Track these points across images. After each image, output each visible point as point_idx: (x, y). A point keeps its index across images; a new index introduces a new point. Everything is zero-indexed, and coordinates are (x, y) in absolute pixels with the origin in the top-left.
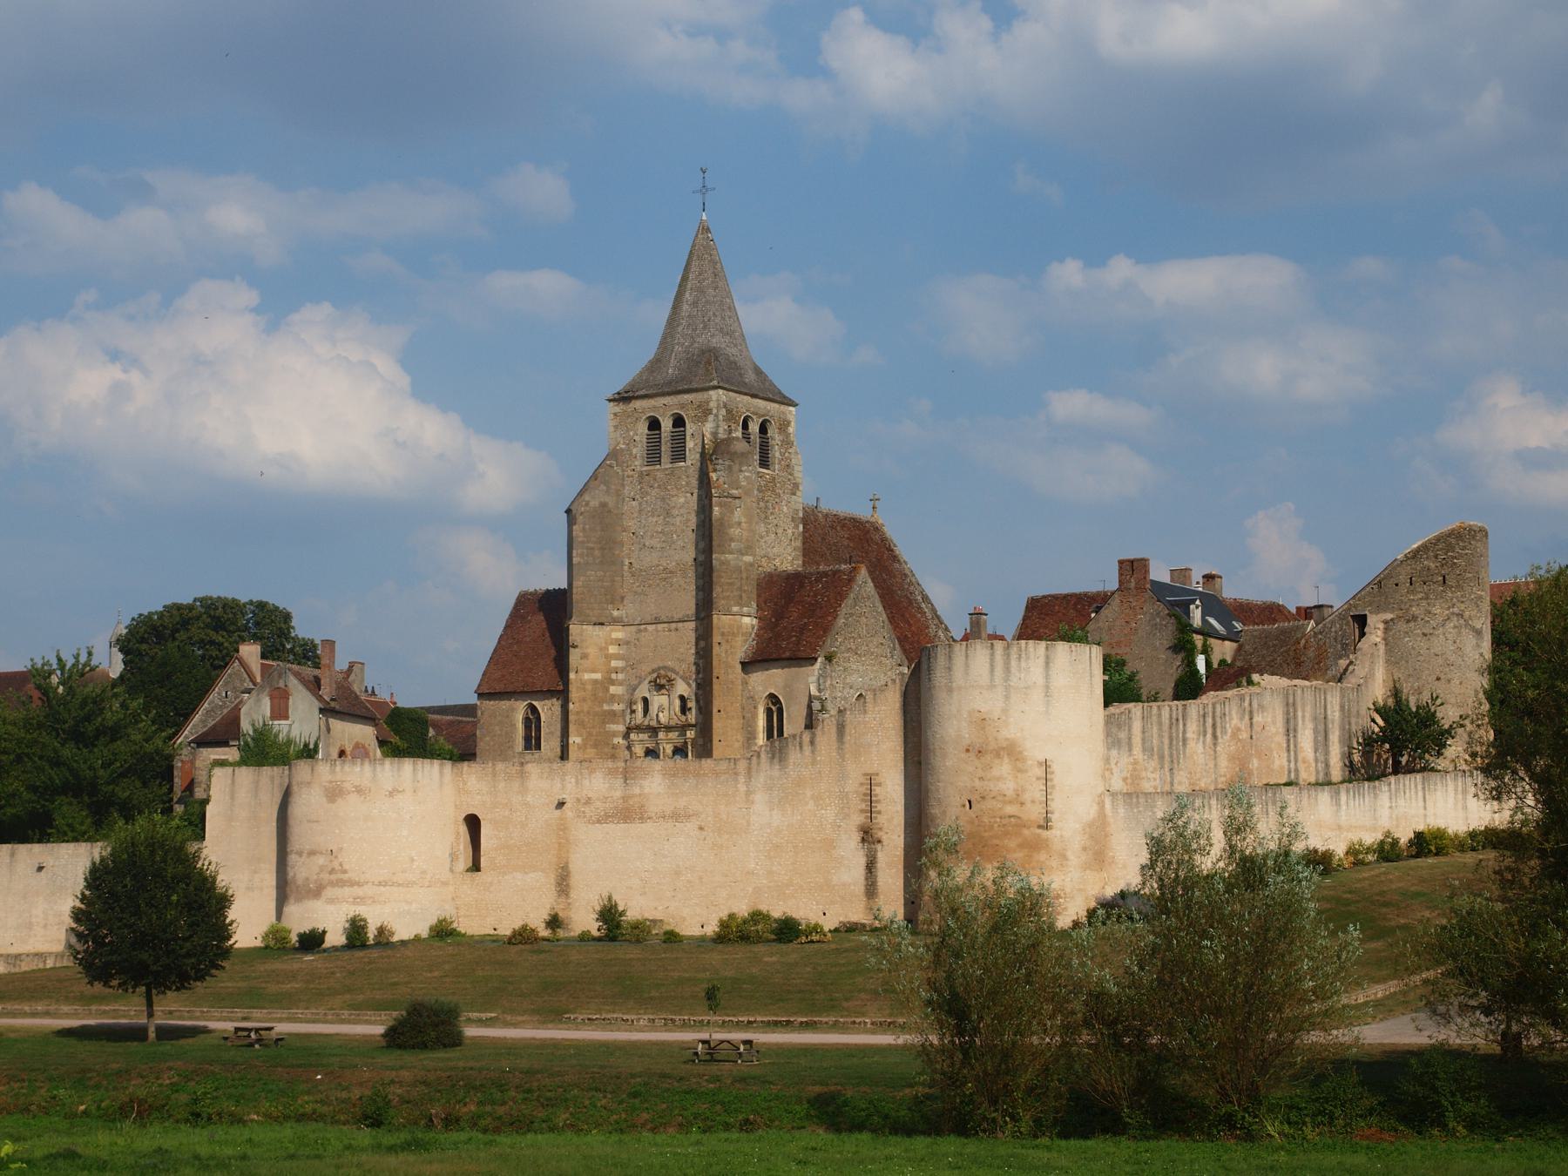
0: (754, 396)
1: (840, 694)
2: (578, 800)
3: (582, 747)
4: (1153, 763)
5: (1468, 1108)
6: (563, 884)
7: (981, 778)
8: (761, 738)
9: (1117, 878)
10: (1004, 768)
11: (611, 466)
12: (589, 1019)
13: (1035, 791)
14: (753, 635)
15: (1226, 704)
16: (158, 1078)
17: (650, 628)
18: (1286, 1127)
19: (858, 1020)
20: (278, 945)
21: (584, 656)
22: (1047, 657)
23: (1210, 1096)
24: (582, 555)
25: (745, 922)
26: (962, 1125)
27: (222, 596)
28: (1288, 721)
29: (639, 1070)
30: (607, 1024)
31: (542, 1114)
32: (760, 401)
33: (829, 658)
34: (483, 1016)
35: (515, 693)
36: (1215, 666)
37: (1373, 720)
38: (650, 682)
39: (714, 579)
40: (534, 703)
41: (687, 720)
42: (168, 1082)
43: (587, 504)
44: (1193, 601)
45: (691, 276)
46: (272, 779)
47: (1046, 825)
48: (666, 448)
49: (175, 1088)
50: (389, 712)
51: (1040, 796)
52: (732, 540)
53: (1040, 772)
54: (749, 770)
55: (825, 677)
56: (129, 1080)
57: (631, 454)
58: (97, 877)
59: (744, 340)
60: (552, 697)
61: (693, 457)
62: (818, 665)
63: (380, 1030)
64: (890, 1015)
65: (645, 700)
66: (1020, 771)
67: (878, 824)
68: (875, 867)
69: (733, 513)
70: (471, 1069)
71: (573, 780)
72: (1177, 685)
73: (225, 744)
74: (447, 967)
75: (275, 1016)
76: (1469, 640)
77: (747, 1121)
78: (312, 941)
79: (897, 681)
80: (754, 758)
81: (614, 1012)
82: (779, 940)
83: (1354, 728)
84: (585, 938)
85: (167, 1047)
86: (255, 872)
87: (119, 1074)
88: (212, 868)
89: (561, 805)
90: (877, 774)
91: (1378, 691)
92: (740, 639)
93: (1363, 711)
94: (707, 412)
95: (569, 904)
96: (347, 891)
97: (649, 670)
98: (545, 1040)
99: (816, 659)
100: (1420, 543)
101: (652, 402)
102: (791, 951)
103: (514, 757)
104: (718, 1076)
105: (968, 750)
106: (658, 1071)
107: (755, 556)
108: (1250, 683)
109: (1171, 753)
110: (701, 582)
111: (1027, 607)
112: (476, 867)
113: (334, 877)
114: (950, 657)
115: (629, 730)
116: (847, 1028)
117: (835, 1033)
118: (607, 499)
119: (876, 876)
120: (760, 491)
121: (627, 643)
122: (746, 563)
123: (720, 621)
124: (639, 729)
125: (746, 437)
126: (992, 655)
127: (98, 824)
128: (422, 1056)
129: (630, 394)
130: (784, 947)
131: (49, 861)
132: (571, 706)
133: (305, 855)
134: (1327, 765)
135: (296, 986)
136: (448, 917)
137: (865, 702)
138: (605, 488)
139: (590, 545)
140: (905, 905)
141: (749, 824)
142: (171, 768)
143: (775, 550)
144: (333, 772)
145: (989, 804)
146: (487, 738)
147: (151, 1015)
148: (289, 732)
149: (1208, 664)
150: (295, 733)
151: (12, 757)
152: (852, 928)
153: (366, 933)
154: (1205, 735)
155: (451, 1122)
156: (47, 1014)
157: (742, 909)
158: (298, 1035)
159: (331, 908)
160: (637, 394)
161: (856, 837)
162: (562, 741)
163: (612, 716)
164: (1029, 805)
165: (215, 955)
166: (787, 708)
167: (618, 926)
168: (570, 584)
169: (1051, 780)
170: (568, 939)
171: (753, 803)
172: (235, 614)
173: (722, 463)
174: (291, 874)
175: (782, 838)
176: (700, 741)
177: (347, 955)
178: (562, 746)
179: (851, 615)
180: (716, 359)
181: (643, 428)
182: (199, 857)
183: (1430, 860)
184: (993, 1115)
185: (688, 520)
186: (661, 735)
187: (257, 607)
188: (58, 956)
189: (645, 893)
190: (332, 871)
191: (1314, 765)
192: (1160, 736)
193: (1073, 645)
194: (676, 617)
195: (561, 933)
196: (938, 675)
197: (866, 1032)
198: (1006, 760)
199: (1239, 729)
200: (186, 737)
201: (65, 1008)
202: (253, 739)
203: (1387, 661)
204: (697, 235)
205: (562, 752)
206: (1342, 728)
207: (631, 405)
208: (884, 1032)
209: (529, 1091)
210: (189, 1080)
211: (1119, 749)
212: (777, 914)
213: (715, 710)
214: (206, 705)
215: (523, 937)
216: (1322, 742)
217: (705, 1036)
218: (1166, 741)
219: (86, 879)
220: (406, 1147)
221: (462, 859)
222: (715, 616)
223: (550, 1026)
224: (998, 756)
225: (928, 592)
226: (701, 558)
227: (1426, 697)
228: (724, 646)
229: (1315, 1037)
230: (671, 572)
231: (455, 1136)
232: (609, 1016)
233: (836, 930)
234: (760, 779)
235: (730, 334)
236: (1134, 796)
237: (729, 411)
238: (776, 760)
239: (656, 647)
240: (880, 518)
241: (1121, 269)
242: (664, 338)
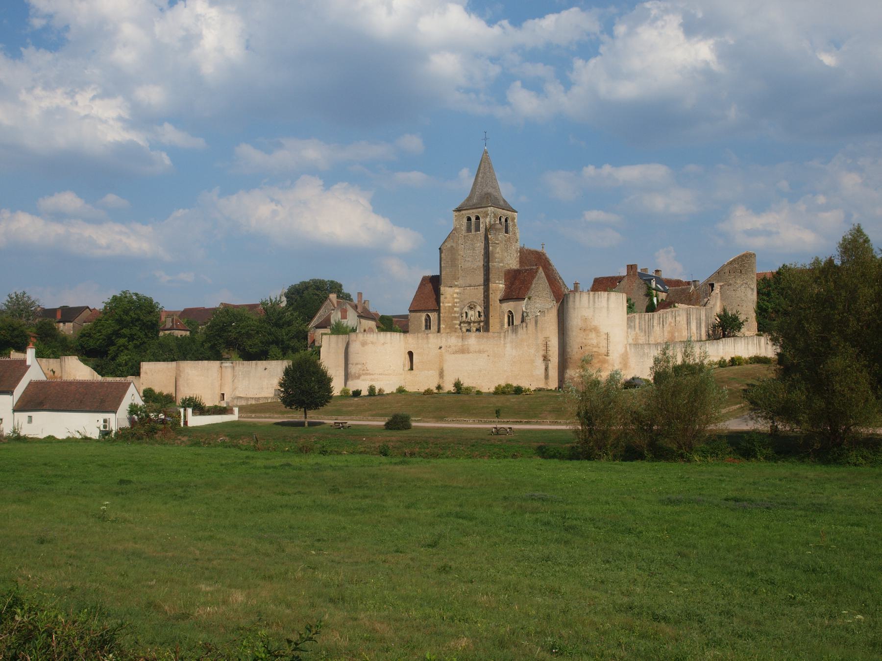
3: (445, 329)
4: (642, 334)
5: (764, 452)
6: (441, 374)
7: (585, 339)
8: (506, 326)
10: (593, 335)
11: (454, 233)
13: (603, 343)
15: (667, 314)
16: (310, 439)
17: (468, 288)
18: (701, 458)
21: (446, 298)
22: (608, 297)
23: (675, 447)
25: (504, 388)
26: (589, 457)
28: (688, 320)
30: (458, 422)
31: (441, 452)
34: (416, 419)
36: (660, 301)
37: (716, 320)
39: (490, 272)
42: (313, 440)
43: (446, 246)
44: (652, 279)
45: (481, 168)
46: (343, 339)
47: (607, 355)
48: (473, 227)
49: (316, 442)
52: (496, 258)
56: (300, 440)
58: (287, 372)
61: (482, 230)
63: (383, 423)
64: (556, 419)
65: (466, 313)
70: (416, 437)
72: (647, 308)
73: (325, 327)
76: (749, 292)
78: (357, 394)
82: (516, 394)
83: (710, 322)
84: (449, 393)
85: (312, 429)
87: (296, 437)
88: (326, 368)
89: (440, 348)
90: (549, 337)
91: (718, 309)
92: (499, 292)
93: (713, 317)
94: (487, 215)
99: (525, 299)
100: (732, 259)
101: (469, 211)
102: (520, 397)
105: (580, 329)
107: (503, 263)
108: (674, 306)
109: (648, 331)
110: (485, 273)
112: (412, 369)
113: (364, 372)
115: (461, 323)
118: (453, 244)
120: (505, 242)
121: (460, 293)
124: (464, 322)
125: (501, 223)
126: (589, 297)
127: (284, 354)
128: (398, 432)
131: (268, 367)
132: (441, 315)
134: (701, 335)
139: (448, 260)
140: (558, 382)
141: (505, 354)
142: (307, 335)
145: (587, 348)
147: (306, 418)
148: (347, 323)
149: (657, 300)
150: (349, 324)
151: (255, 332)
152: (540, 390)
154: (660, 324)
155: (412, 454)
156: (270, 417)
157: (503, 383)
161: (542, 359)
163: (455, 318)
164: (602, 348)
167: (461, 389)
174: (349, 371)
176: (485, 326)
177: (369, 398)
180: (490, 197)
181: (465, 220)
183: (736, 367)
184: (600, 453)
185: (481, 252)
186: (472, 324)
188: (272, 398)
190: (363, 370)
191: (696, 334)
192: (645, 325)
194: (477, 285)
195: (441, 391)
197: (548, 425)
198: (594, 332)
199: (671, 323)
200: (312, 325)
201: (276, 416)
203: (721, 299)
206: (706, 322)
208: (554, 425)
209: (437, 444)
212: (515, 385)
213: (490, 316)
215: (428, 392)
216: (699, 327)
217: (495, 426)
218: (647, 326)
219: (756, 312)
220: (401, 463)
221: (407, 366)
222: (490, 284)
223: (439, 422)
224: (591, 331)
226: (485, 264)
227: (734, 312)
229: (712, 427)
233: (535, 390)
234: (509, 339)
235: (495, 188)
237: (495, 214)
238: (514, 333)
240: (545, 251)
241: (607, 169)
242: (472, 190)
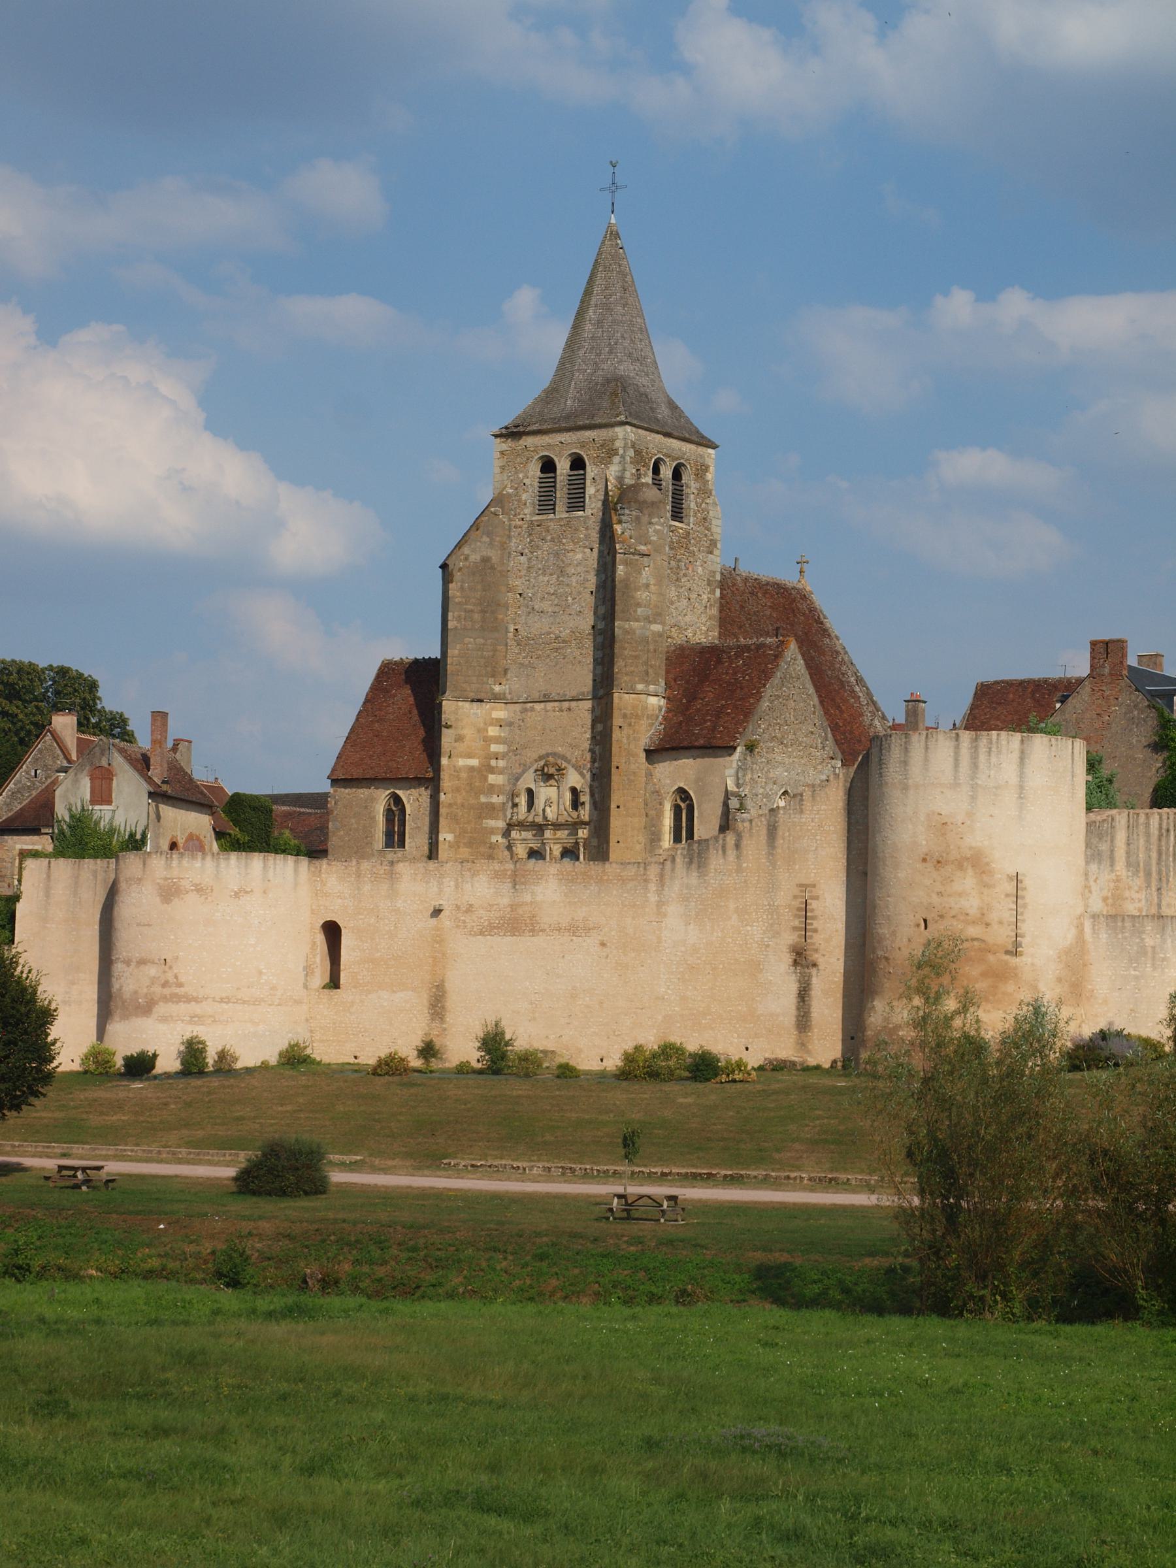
0: (667, 435)
1: (761, 791)
2: (458, 907)
3: (455, 845)
4: (1139, 882)
6: (437, 1006)
7: (940, 894)
8: (667, 840)
9: (1096, 1016)
10: (967, 882)
12: (472, 1166)
13: (1003, 910)
14: (660, 718)
17: (538, 707)
19: (793, 1175)
20: (100, 1070)
21: (459, 739)
22: (1022, 752)
24: (459, 619)
27: (17, 659)
29: (544, 1227)
30: (494, 1172)
32: (675, 441)
33: (751, 748)
35: (375, 779)
38: (536, 771)
40: (397, 792)
41: (578, 816)
43: (466, 559)
45: (596, 290)
46: (95, 873)
48: (561, 495)
50: (227, 799)
51: (1009, 917)
52: (638, 605)
53: (1010, 888)
54: (662, 876)
55: (745, 770)
57: (519, 501)
59: (657, 368)
60: (419, 786)
62: (737, 755)
63: (231, 1172)
64: (831, 1170)
65: (530, 793)
66: (986, 886)
67: (813, 944)
68: (809, 996)
69: (640, 573)
70: (344, 1221)
71: (452, 883)
72: (1155, 790)
73: (35, 831)
74: (301, 1100)
75: (97, 1152)
77: (684, 1292)
79: (841, 776)
80: (668, 863)
81: (501, 1158)
82: (694, 1078)
84: (463, 1070)
86: (74, 984)
88: (33, 976)
89: (437, 912)
90: (814, 886)
92: (644, 722)
94: (612, 452)
95: (445, 1029)
96: (182, 1007)
97: (535, 756)
98: (424, 1189)
99: (735, 748)
102: (709, 1092)
103: (373, 855)
104: (639, 1237)
105: (924, 860)
106: (568, 1230)
111: (976, 694)
112: (334, 982)
113: (167, 991)
114: (906, 748)
115: (510, 826)
116: (781, 1184)
117: (766, 1189)
119: (810, 1006)
121: (511, 724)
122: (654, 633)
123: (622, 700)
124: (522, 825)
125: (657, 483)
126: (957, 748)
128: (282, 1205)
129: (521, 429)
130: (700, 1086)
132: (442, 796)
133: (133, 964)
135: (123, 1118)
136: (301, 1042)
137: (802, 800)
138: (488, 540)
139: (470, 607)
140: (843, 1040)
141: (659, 942)
143: (687, 619)
144: (169, 867)
146: (342, 833)
148: (113, 817)
150: (119, 821)
153: (205, 1058)
155: (328, 1283)
157: (651, 1041)
158: (130, 1176)
159: (162, 1027)
160: (529, 429)
161: (788, 959)
162: (431, 838)
163: (490, 810)
164: (995, 926)
165: (34, 1079)
166: (699, 806)
167: (503, 1056)
168: (444, 652)
169: (1023, 898)
170: (444, 1071)
171: (665, 915)
172: (31, 681)
173: (628, 513)
174: (116, 986)
175: (699, 958)
177: (182, 1083)
178: (430, 844)
179: (778, 697)
180: (624, 389)
181: (534, 469)
182: (17, 963)
184: (982, 1292)
186: (548, 834)
187: (57, 673)
189: (535, 1019)
190: (165, 984)
192: (1148, 849)
193: (1053, 738)
195: (435, 1064)
196: (891, 770)
197: (805, 1189)
198: (970, 872)
202: (69, 826)
204: (603, 242)
205: (430, 851)
207: (521, 442)
209: (414, 1249)
210: (7, 1226)
211: (1100, 863)
212: (692, 1047)
213: (613, 806)
214: (11, 785)
215: (390, 1067)
217: (620, 1190)
218: (1154, 855)
220: (289, 1313)
222: (616, 695)
223: (426, 1172)
224: (960, 867)
225: (863, 673)
226: (601, 625)
228: (626, 730)
230: (564, 642)
231: (334, 1302)
232: (495, 1163)
233: (761, 1068)
234: (675, 888)
235: (640, 360)
236: (1119, 919)
237: (638, 452)
238: (694, 866)
239: (544, 730)
